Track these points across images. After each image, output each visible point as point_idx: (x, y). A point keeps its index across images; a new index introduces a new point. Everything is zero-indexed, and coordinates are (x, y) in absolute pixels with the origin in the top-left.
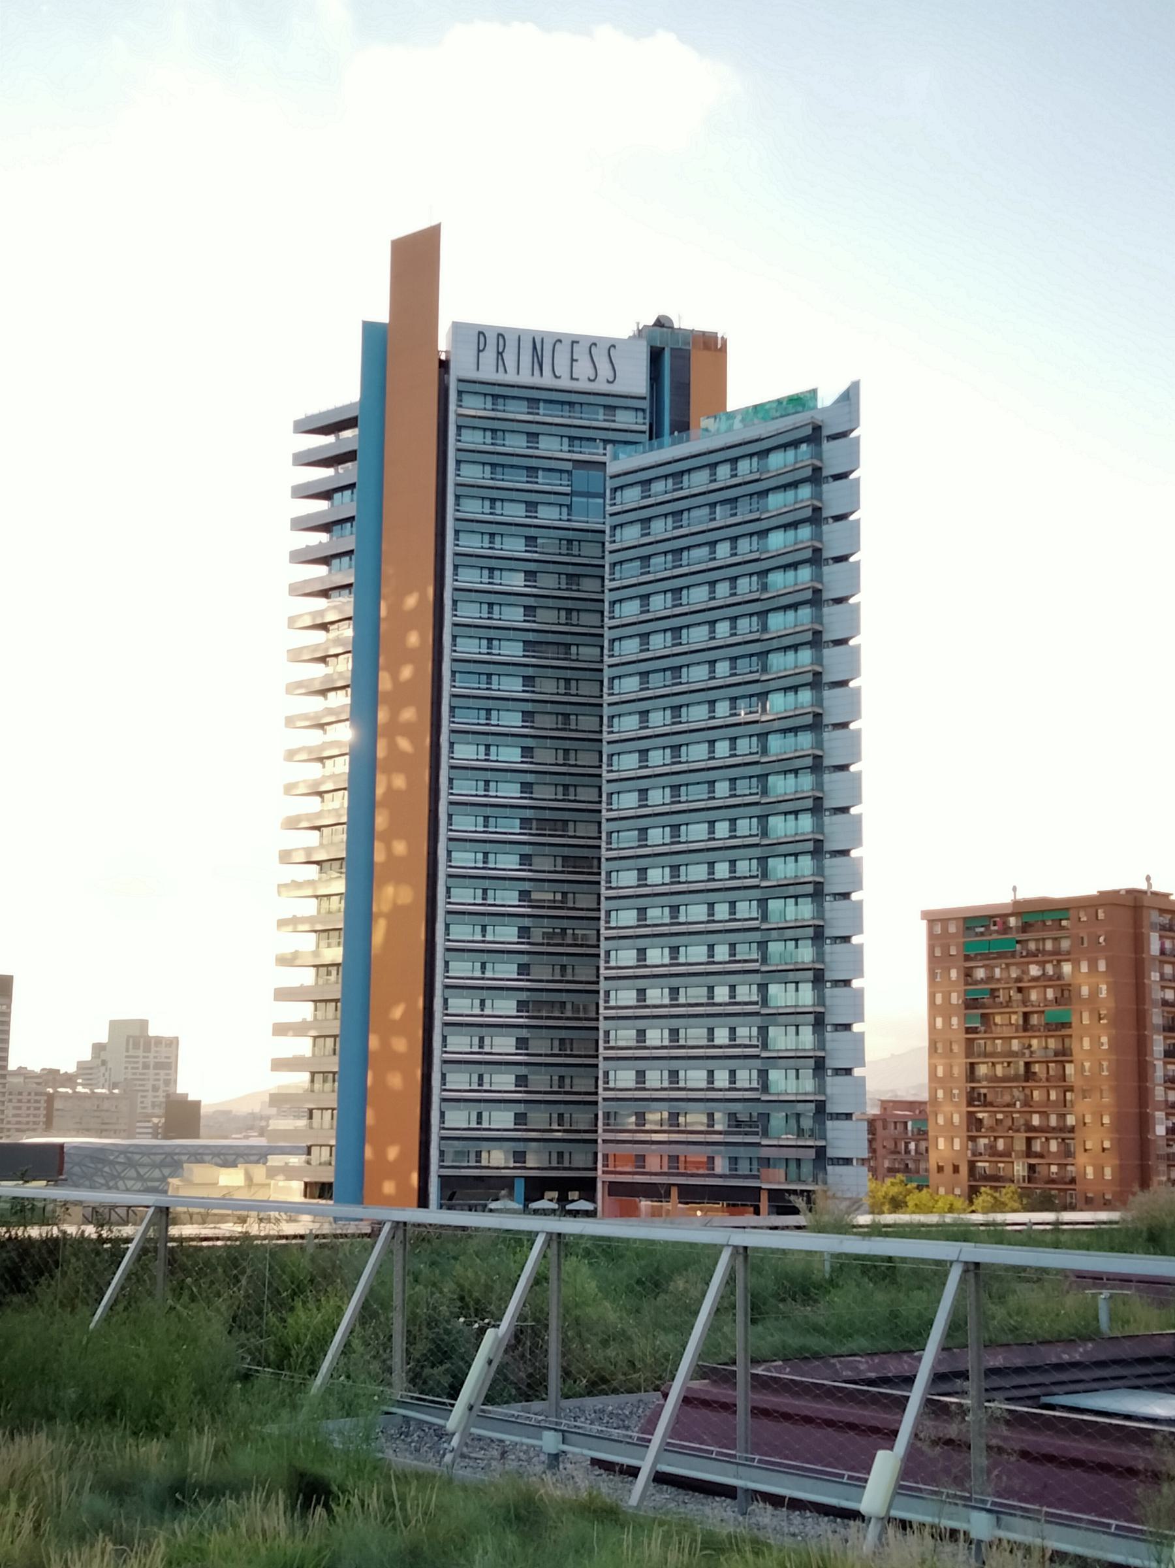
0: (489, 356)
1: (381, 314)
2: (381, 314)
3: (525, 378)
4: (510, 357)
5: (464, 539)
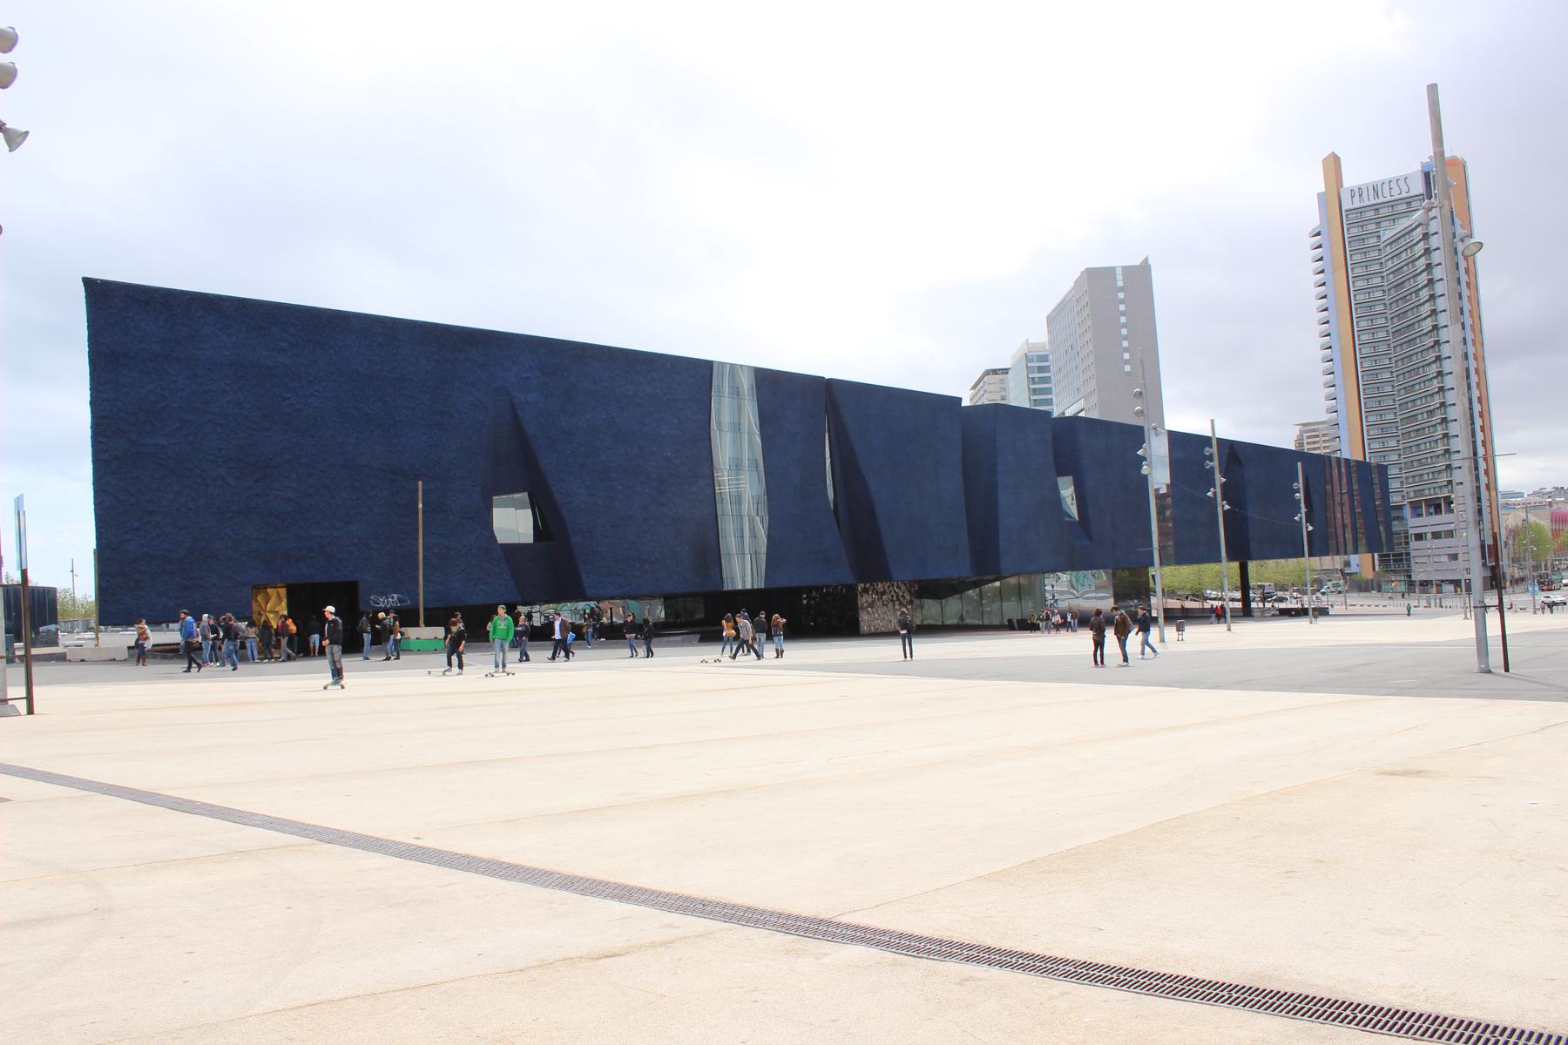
0: (1357, 198)
1: (1323, 189)
2: (1323, 189)
3: (1372, 202)
4: (1365, 196)
5: (1352, 231)
